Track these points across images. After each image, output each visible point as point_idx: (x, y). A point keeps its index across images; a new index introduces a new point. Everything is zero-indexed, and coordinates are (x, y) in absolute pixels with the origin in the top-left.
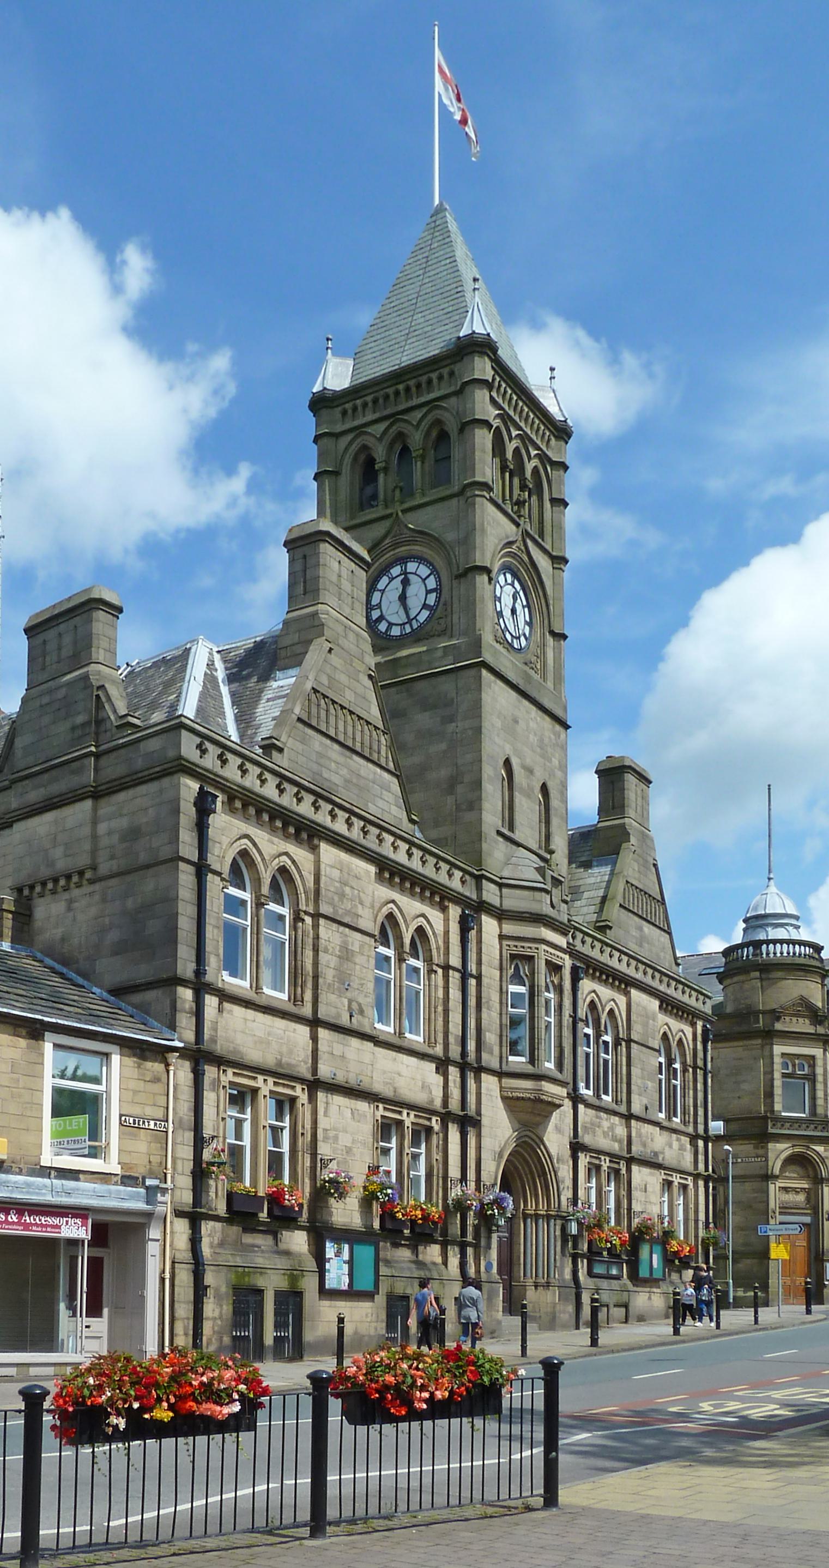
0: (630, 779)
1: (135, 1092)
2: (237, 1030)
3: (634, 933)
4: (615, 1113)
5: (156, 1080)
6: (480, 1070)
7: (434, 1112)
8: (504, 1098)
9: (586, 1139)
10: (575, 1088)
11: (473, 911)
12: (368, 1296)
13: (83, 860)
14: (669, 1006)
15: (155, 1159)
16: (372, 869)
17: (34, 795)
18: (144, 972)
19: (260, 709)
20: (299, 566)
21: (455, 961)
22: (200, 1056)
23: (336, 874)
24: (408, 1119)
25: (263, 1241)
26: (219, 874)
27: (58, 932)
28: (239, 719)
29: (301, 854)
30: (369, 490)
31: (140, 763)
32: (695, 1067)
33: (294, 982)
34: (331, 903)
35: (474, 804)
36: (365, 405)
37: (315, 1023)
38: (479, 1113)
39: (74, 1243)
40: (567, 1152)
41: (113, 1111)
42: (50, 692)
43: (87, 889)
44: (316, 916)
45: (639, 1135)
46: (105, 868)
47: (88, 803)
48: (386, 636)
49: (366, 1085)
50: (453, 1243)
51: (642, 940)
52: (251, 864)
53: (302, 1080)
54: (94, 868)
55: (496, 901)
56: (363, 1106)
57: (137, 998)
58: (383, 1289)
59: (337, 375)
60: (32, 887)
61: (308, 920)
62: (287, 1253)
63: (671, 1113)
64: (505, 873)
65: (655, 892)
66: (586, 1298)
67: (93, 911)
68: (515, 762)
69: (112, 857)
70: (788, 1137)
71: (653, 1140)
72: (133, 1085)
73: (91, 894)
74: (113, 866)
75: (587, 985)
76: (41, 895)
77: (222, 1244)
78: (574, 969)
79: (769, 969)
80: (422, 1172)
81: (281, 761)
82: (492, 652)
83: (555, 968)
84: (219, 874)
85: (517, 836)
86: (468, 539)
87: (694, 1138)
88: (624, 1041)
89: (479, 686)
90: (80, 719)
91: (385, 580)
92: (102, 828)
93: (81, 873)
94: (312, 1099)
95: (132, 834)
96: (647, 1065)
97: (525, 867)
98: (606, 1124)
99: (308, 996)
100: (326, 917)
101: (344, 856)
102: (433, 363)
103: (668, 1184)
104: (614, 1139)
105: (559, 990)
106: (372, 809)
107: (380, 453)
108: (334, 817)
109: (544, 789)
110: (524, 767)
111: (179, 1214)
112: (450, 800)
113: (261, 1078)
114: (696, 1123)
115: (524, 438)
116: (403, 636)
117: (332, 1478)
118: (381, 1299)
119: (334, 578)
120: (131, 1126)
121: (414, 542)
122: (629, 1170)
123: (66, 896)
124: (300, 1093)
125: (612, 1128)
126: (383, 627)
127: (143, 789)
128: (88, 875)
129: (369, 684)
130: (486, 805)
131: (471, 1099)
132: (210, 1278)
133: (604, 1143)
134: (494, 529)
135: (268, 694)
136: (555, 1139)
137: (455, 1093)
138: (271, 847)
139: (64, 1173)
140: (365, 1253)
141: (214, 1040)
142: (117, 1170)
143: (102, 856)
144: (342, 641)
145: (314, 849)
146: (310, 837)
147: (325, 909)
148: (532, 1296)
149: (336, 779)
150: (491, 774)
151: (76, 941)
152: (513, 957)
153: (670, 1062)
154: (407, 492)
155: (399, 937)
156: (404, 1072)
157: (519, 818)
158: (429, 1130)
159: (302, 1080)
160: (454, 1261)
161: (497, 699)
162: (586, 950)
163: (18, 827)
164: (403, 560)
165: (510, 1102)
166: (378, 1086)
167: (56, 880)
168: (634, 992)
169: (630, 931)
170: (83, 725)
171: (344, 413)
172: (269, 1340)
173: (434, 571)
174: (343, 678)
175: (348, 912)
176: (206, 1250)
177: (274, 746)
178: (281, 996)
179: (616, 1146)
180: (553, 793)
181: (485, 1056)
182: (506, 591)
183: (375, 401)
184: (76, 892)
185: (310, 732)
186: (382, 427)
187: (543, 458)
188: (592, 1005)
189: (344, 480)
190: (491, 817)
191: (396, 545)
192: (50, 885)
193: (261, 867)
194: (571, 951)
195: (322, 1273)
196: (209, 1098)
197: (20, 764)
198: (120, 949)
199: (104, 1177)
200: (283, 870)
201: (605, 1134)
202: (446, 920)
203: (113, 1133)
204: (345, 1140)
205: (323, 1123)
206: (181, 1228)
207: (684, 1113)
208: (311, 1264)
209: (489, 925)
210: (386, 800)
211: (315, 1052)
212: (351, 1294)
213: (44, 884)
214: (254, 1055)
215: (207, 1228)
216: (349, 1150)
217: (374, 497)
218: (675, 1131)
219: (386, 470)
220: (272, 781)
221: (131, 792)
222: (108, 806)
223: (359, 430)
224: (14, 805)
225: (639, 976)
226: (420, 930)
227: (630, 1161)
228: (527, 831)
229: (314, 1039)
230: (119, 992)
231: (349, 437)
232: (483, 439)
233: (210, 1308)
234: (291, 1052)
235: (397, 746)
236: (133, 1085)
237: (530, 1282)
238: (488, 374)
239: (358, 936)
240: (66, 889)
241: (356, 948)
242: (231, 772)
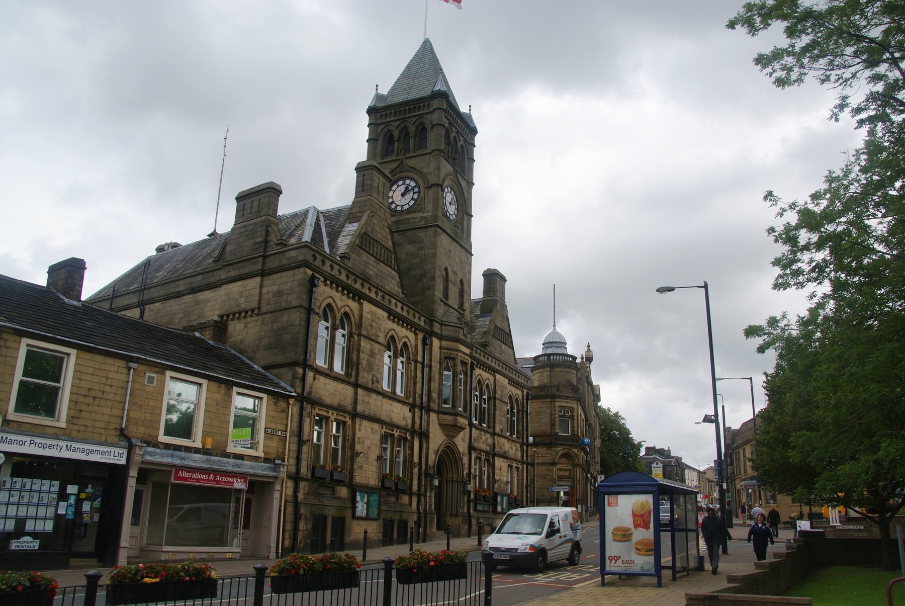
1: (273, 417)
2: (326, 389)
3: (498, 348)
4: (488, 432)
5: (283, 411)
6: (429, 410)
7: (407, 430)
8: (440, 424)
9: (476, 445)
10: (470, 421)
11: (429, 335)
13: (254, 305)
14: (512, 382)
15: (280, 450)
16: (386, 315)
17: (233, 273)
19: (339, 240)
20: (361, 179)
21: (420, 359)
22: (306, 400)
23: (369, 316)
24: (396, 434)
25: (327, 492)
26: (317, 314)
27: (239, 338)
28: (330, 243)
29: (354, 305)
30: (390, 148)
31: (285, 262)
32: (523, 412)
34: (366, 330)
35: (431, 288)
36: (391, 113)
37: (356, 386)
38: (428, 431)
39: (239, 491)
40: (466, 451)
41: (262, 426)
42: (246, 226)
43: (255, 318)
44: (360, 335)
45: (498, 443)
46: (264, 309)
47: (258, 279)
48: (394, 210)
49: (378, 416)
50: (415, 494)
51: (501, 352)
52: (332, 310)
53: (349, 413)
54: (259, 308)
55: (438, 331)
56: (376, 426)
58: (382, 516)
60: (228, 316)
61: (356, 337)
62: (339, 498)
63: (512, 433)
64: (444, 319)
65: (507, 331)
66: (474, 522)
67: (257, 329)
68: (449, 269)
69: (268, 304)
70: (562, 445)
71: (505, 445)
72: (272, 413)
73: (257, 321)
74: (269, 308)
75: (478, 371)
76: (233, 320)
77: (308, 494)
78: (472, 364)
80: (402, 459)
83: (464, 364)
84: (317, 314)
85: (450, 302)
87: (522, 445)
90: (258, 240)
91: (395, 186)
92: (265, 290)
93: (253, 311)
94: (354, 423)
95: (279, 294)
96: (502, 409)
97: (453, 317)
98: (484, 438)
99: (354, 373)
100: (364, 336)
101: (373, 308)
102: (422, 100)
103: (510, 466)
104: (487, 445)
105: (466, 374)
106: (387, 287)
107: (396, 133)
108: (370, 290)
109: (461, 281)
110: (453, 272)
111: (289, 477)
113: (330, 412)
114: (523, 438)
116: (402, 211)
117: (382, 580)
118: (381, 522)
119: (376, 185)
120: (269, 434)
121: (409, 171)
122: (494, 460)
123: (244, 321)
125: (486, 440)
126: (393, 206)
127: (286, 273)
128: (256, 312)
129: (388, 231)
130: (437, 288)
131: (424, 424)
132: (302, 511)
133: (483, 447)
135: (343, 233)
137: (418, 421)
138: (343, 302)
140: (375, 498)
141: (310, 393)
142: (261, 454)
143: (264, 303)
144: (378, 213)
146: (359, 299)
147: (364, 332)
148: (449, 521)
149: (371, 273)
151: (247, 343)
152: (446, 358)
153: (512, 408)
154: (407, 150)
155: (396, 347)
156: (395, 410)
157: (451, 294)
158: (405, 439)
159: (349, 413)
160: (414, 504)
162: (478, 356)
163: (224, 287)
164: (404, 179)
165: (443, 426)
166: (384, 418)
167: (240, 313)
168: (498, 376)
169: (496, 347)
170: (260, 242)
171: (382, 116)
172: (328, 542)
174: (377, 228)
175: (374, 334)
176: (301, 496)
177: (345, 257)
179: (488, 448)
180: (465, 284)
181: (432, 404)
183: (395, 112)
184: (249, 319)
185: (362, 251)
186: (398, 123)
187: (465, 141)
188: (479, 382)
189: (380, 143)
190: (438, 293)
191: (401, 172)
192: (237, 316)
193: (336, 312)
194: (470, 356)
195: (354, 508)
196: (307, 421)
197: (228, 258)
198: (268, 347)
199: (255, 459)
200: (346, 314)
201: (483, 443)
202: (417, 339)
203: (261, 436)
204: (368, 443)
205: (358, 434)
206: (290, 484)
207: (518, 433)
208: (349, 504)
209: (436, 342)
210: (393, 285)
212: (367, 518)
213: (234, 314)
214: (328, 400)
215: (302, 484)
216: (369, 448)
217: (393, 151)
218: (514, 441)
219: (398, 141)
220: (359, 281)
221: (279, 275)
223: (388, 124)
224: (223, 277)
225: (500, 368)
226: (405, 344)
228: (453, 301)
229: (356, 394)
231: (383, 126)
233: (302, 526)
234: (345, 399)
236: (272, 413)
237: (448, 514)
238: (445, 106)
239: (377, 346)
240: (245, 317)
241: (377, 351)
242: (327, 268)
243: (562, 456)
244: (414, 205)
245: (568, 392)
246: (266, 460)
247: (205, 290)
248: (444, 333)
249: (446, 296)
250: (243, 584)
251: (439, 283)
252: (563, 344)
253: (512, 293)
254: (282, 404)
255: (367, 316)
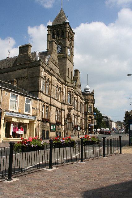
0: (78, 72)
12: (55, 131)
18: (34, 90)
27: (21, 84)
29: (50, 77)
33: (49, 92)
35: (65, 73)
37: (51, 97)
39: (26, 124)
44: (51, 84)
47: (27, 69)
57: (33, 93)
59: (51, 24)
67: (27, 82)
79: (87, 95)
81: (49, 66)
82: (67, 56)
86: (65, 44)
88: (77, 102)
89: (66, 60)
93: (25, 77)
95: (33, 73)
112: (63, 72)
115: (71, 34)
124: (49, 106)
134: (68, 43)
136: (71, 113)
138: (48, 76)
139: (26, 115)
145: (51, 76)
147: (52, 84)
150: (67, 69)
161: (68, 61)
173: (61, 47)
178: (47, 94)
182: (68, 50)
187: (72, 36)
190: (67, 75)
199: (30, 115)
211: (51, 101)
214: (45, 101)
222: (29, 69)
227: (77, 116)
229: (51, 99)
230: (30, 92)
232: (67, 33)
235: (59, 65)
243: (89, 117)
244: (60, 52)
245: (91, 101)
246: (33, 116)
247: (10, 72)
248: (68, 85)
249: (68, 75)
250: (89, 156)
251: (67, 71)
252: (12, 95)
253: (81, 76)
254: (36, 101)
255: (53, 80)
